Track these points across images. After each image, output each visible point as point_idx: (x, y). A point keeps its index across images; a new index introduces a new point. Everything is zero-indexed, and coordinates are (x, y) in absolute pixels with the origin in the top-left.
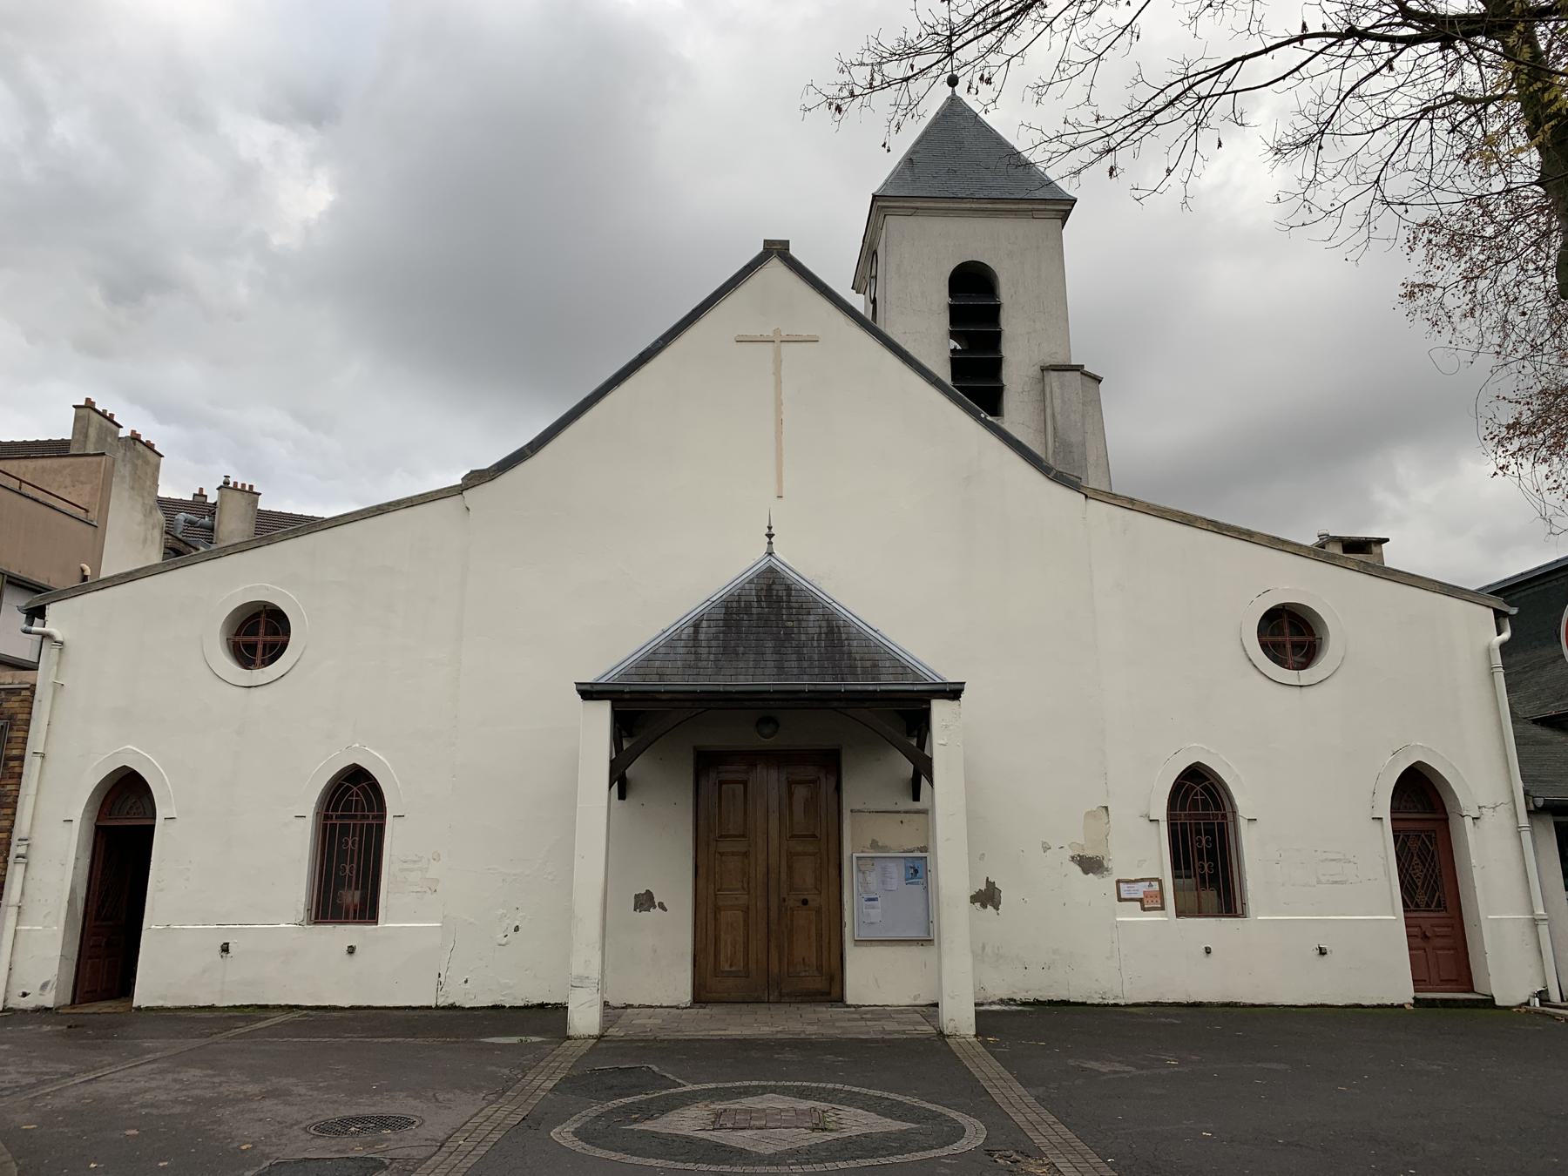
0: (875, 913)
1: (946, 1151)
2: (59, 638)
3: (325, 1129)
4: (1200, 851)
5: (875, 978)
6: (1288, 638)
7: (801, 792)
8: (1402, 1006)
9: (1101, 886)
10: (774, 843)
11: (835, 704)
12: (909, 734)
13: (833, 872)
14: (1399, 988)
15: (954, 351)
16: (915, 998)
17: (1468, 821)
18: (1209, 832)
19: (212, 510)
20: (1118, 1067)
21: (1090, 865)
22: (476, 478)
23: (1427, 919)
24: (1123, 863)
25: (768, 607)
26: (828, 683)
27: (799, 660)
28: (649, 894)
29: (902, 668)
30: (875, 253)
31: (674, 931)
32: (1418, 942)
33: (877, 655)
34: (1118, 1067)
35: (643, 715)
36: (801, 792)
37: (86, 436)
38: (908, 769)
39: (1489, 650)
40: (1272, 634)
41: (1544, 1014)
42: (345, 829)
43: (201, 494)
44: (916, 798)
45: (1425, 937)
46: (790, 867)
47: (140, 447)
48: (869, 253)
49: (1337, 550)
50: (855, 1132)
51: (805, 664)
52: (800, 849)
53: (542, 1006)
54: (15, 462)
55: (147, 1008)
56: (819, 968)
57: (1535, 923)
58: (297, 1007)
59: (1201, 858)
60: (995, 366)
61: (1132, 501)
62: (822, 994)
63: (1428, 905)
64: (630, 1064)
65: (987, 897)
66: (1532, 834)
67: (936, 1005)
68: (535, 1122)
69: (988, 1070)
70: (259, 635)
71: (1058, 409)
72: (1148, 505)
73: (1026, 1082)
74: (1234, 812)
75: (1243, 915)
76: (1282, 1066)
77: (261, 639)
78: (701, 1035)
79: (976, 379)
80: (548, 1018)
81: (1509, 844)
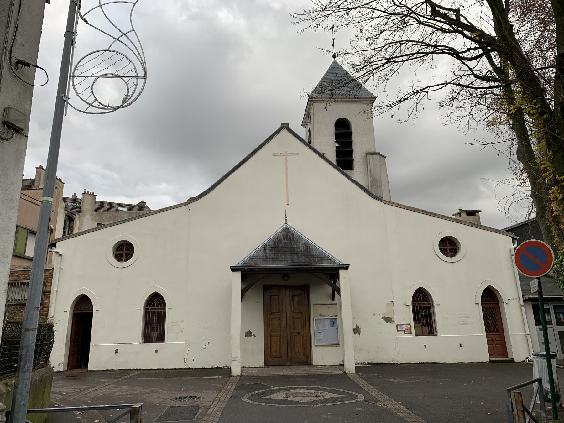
0: (321, 336)
1: (354, 401)
4: (422, 315)
5: (322, 357)
6: (448, 247)
7: (296, 298)
8: (486, 362)
10: (288, 315)
12: (331, 279)
13: (307, 324)
14: (485, 357)
15: (336, 147)
16: (335, 363)
17: (505, 304)
18: (425, 309)
20: (399, 380)
21: (388, 320)
24: (398, 319)
25: (287, 241)
26: (307, 265)
27: (298, 258)
29: (330, 260)
30: (309, 114)
31: (258, 344)
32: (490, 342)
33: (322, 256)
34: (399, 380)
35: (252, 276)
36: (296, 298)
37: (40, 178)
38: (330, 290)
39: (510, 250)
40: (443, 246)
41: (529, 364)
42: (153, 313)
43: (75, 195)
44: (333, 300)
45: (493, 341)
46: (294, 323)
47: (58, 181)
48: (308, 115)
49: (464, 215)
50: (327, 397)
51: (300, 259)
52: (296, 316)
53: (217, 368)
54: (27, 191)
55: (94, 371)
56: (304, 355)
57: (526, 335)
58: (138, 370)
59: (423, 317)
60: (350, 153)
61: (398, 204)
62: (304, 362)
63: (493, 331)
64: (250, 382)
65: (357, 331)
66: (525, 308)
67: (343, 365)
69: (361, 382)
70: (124, 251)
71: (372, 167)
72: (404, 206)
73: (373, 385)
74: (433, 302)
75: (436, 335)
77: (124, 252)
78: (271, 375)
79: (344, 161)
80: (225, 371)
81: (518, 311)
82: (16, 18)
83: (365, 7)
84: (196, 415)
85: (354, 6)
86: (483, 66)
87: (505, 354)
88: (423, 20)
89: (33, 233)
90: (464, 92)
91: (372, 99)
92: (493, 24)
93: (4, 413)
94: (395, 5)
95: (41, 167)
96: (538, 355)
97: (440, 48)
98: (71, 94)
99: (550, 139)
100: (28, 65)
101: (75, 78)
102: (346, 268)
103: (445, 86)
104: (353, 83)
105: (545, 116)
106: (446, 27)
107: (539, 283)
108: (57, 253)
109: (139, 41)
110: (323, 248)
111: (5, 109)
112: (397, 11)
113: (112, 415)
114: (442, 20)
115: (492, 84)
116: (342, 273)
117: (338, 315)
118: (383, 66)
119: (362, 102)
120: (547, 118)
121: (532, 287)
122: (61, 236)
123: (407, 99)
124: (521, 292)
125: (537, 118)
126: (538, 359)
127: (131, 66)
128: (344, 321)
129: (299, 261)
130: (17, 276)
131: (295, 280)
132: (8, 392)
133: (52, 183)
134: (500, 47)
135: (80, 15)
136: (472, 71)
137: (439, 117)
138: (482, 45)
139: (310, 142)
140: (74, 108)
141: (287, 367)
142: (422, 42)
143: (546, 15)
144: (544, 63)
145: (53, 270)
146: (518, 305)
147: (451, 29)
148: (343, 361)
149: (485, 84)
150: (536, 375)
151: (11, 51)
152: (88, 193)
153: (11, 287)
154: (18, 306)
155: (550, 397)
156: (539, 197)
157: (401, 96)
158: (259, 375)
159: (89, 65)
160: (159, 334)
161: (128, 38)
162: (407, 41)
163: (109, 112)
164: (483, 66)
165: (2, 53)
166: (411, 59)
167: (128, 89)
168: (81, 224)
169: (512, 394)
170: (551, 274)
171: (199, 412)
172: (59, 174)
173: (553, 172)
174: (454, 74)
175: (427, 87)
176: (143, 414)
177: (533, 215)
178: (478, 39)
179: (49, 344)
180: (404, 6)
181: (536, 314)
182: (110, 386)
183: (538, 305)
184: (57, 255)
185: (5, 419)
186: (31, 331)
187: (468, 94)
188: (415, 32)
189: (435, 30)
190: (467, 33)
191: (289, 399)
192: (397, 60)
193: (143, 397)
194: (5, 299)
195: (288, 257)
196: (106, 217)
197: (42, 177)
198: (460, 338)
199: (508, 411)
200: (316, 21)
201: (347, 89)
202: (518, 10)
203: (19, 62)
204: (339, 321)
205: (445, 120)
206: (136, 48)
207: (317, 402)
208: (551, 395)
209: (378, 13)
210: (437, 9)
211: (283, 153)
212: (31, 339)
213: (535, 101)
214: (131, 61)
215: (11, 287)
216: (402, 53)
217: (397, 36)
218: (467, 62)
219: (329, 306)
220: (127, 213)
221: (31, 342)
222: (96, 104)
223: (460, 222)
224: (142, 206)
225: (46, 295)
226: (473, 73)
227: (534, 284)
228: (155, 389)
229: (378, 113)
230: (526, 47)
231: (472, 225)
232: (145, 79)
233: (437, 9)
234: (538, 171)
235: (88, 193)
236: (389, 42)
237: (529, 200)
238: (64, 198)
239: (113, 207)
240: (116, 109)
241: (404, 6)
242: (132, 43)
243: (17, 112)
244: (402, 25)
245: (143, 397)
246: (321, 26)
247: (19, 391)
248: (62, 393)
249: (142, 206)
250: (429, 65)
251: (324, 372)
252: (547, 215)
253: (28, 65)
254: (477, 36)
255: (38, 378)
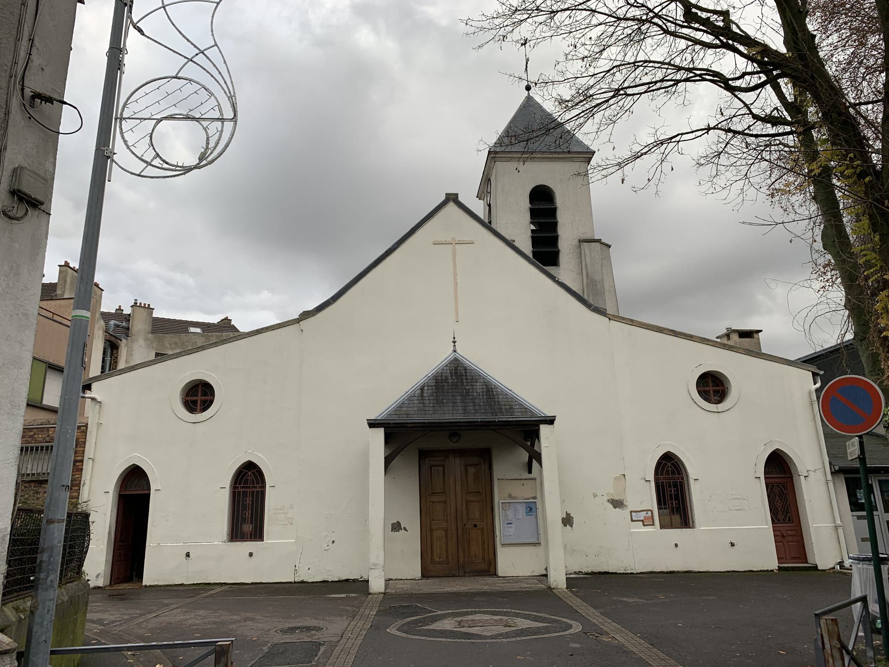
0: (511, 530)
1: (566, 633)
2: (99, 400)
3: (285, 631)
4: (671, 495)
5: (513, 563)
8: (772, 571)
9: (622, 514)
11: (493, 427)
12: (526, 440)
13: (489, 510)
14: (772, 563)
15: (532, 231)
16: (533, 572)
17: (802, 478)
18: (675, 486)
19: (128, 318)
21: (617, 504)
22: (306, 315)
23: (784, 527)
24: (633, 503)
25: (455, 379)
26: (489, 418)
28: (399, 524)
29: (525, 409)
30: (489, 180)
31: (411, 542)
32: (780, 539)
33: (512, 403)
35: (404, 436)
36: (472, 470)
37: (65, 281)
38: (525, 456)
39: (810, 393)
41: (841, 572)
43: (120, 309)
44: (530, 472)
45: (783, 536)
46: (467, 509)
48: (486, 180)
50: (524, 627)
51: (477, 408)
52: (472, 499)
53: (347, 580)
56: (484, 559)
57: (836, 528)
59: (671, 499)
60: (554, 240)
61: (632, 321)
63: (784, 520)
64: (399, 603)
65: (567, 521)
66: (834, 483)
67: (546, 576)
68: (376, 627)
70: (199, 396)
71: (588, 262)
72: (640, 323)
74: (687, 476)
75: (693, 527)
76: (713, 598)
77: (199, 398)
78: (433, 591)
79: (545, 252)
80: (360, 586)
81: (823, 488)
82: (30, 25)
83: (580, 7)
84: (316, 655)
85: (562, 7)
86: (767, 100)
87: (803, 557)
88: (672, 27)
89: (59, 370)
90: (737, 141)
91: (588, 155)
92: (782, 33)
93: (14, 655)
94: (628, 4)
95: (67, 265)
96: (859, 559)
97: (698, 72)
98: (118, 146)
99: (879, 218)
100: (50, 100)
101: (123, 122)
102: (550, 421)
103: (707, 133)
104: (559, 130)
105: (867, 179)
106: (708, 38)
107: (861, 444)
108: (93, 399)
109: (225, 62)
110: (513, 390)
111: (15, 171)
112: (629, 15)
113: (183, 656)
114: (701, 27)
115: (781, 129)
116: (544, 429)
117: (538, 496)
118: (607, 101)
119: (572, 160)
120: (870, 182)
121: (848, 451)
122: (99, 373)
123: (645, 153)
124: (827, 459)
125: (855, 183)
126: (859, 566)
127: (213, 102)
128: (547, 505)
129: (476, 412)
130: (31, 436)
131: (467, 441)
132: (20, 620)
133: (89, 288)
134: (795, 70)
135: (132, 22)
136: (749, 109)
137: (695, 181)
138: (764, 68)
139: (490, 222)
140: (122, 168)
141: (457, 580)
142: (669, 64)
143: (862, 21)
144: (864, 93)
145: (86, 426)
146: (823, 479)
147: (718, 42)
148: (546, 569)
149: (770, 129)
150: (857, 591)
151: (23, 77)
152: (140, 306)
153: (31, 453)
154: (33, 484)
155: (880, 626)
156: (858, 308)
157: (637, 148)
158: (414, 592)
159: (143, 103)
160: (256, 527)
161: (208, 58)
162: (645, 62)
163: (175, 176)
164: (767, 100)
165: (9, 81)
166: (653, 91)
167: (208, 139)
168: (130, 354)
169: (823, 621)
170: (881, 430)
171: (321, 652)
172: (99, 278)
173: (881, 267)
174: (722, 114)
175: (678, 135)
176: (235, 653)
177: (850, 336)
178: (759, 58)
179: (84, 543)
180: (643, 6)
181: (852, 495)
182: (179, 610)
183: (854, 479)
184: (94, 403)
185: (16, 663)
186: (56, 524)
187: (744, 145)
188: (657, 47)
189: (690, 43)
190: (741, 48)
191: (462, 630)
192: (629, 91)
193: (231, 627)
194: (16, 472)
195: (459, 404)
196: (169, 343)
197: (68, 279)
198: (731, 532)
199: (816, 649)
200: (502, 32)
201: (549, 139)
202: (818, 14)
203: (37, 96)
204: (539, 505)
205: (706, 187)
206: (220, 73)
207: (507, 635)
208: (882, 623)
209: (602, 18)
210: (694, 10)
211: (449, 240)
212: (56, 536)
213: (852, 155)
214: (212, 94)
215: (31, 453)
216: (638, 81)
217: (630, 54)
218: (742, 95)
219: (523, 482)
220: (203, 336)
221: (56, 542)
222: (157, 162)
223: (730, 348)
224: (226, 325)
225: (78, 466)
226: (751, 113)
227: (853, 445)
228: (249, 615)
229: (599, 177)
230: (831, 69)
231: (749, 352)
232: (236, 122)
233: (694, 10)
234: (856, 266)
235: (140, 306)
236: (616, 63)
237: (841, 312)
238: (103, 314)
239: (181, 327)
240: (187, 170)
241: (643, 6)
242: (215, 66)
243: (33, 175)
244: (637, 38)
245: (231, 627)
246: (509, 38)
247: (37, 619)
248: (103, 621)
249: (226, 325)
250: (680, 100)
251: (515, 587)
252: (872, 335)
253: (50, 100)
254: (758, 53)
255: (66, 598)
